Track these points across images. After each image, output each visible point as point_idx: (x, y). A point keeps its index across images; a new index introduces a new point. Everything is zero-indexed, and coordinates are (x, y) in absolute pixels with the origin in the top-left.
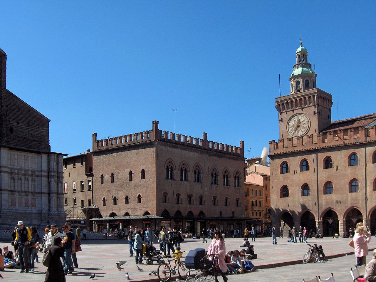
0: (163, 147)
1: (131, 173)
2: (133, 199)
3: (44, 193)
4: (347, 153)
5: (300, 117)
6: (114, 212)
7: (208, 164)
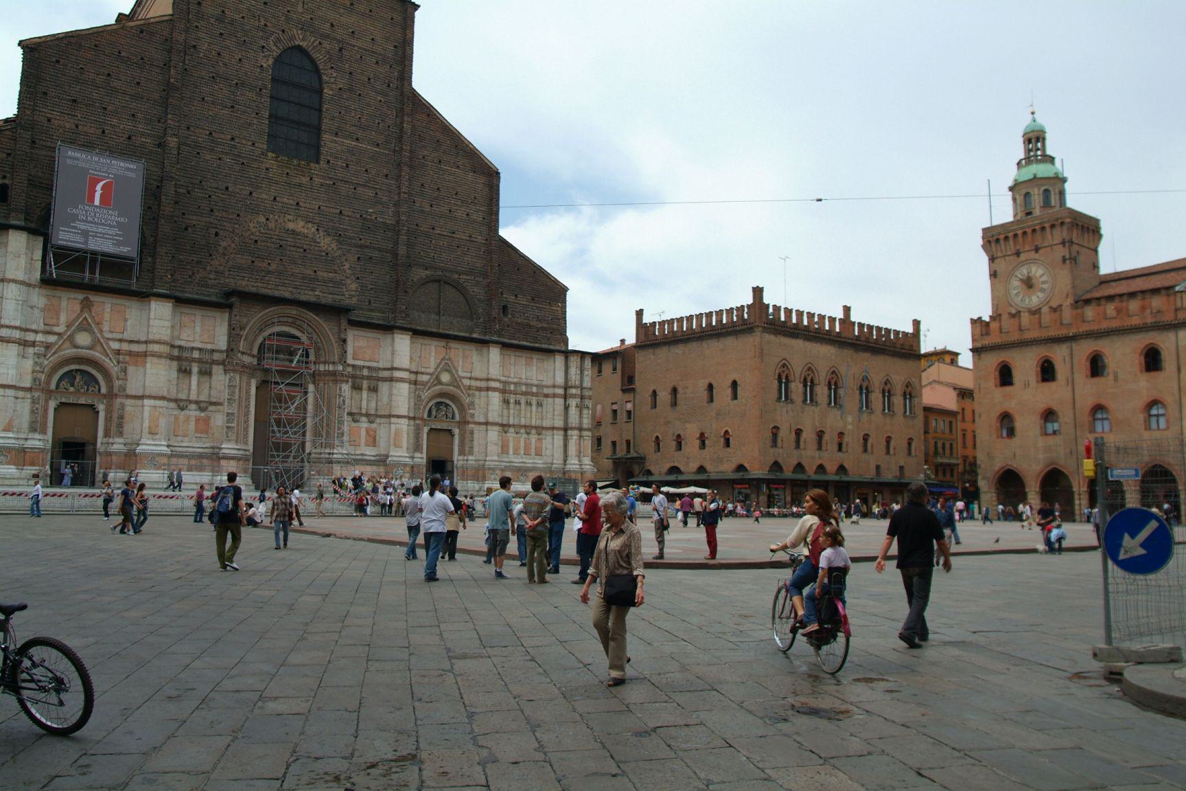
0: (772, 337)
2: (714, 442)
3: (558, 429)
5: (1034, 269)
7: (853, 367)
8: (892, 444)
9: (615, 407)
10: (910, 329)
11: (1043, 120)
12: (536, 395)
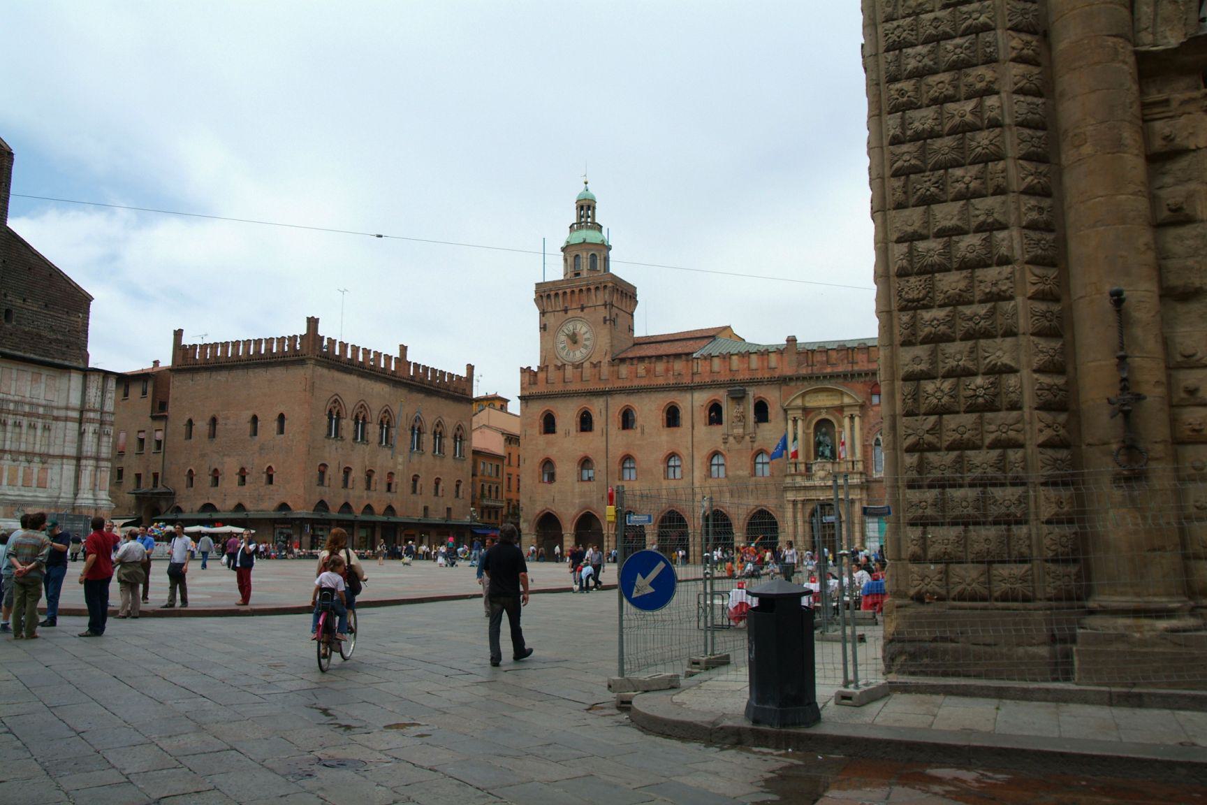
0: (325, 371)
1: (255, 419)
3: (68, 457)
4: (662, 400)
6: (211, 501)
7: (406, 407)
8: (441, 485)
9: (142, 435)
10: (464, 374)
11: (594, 191)
12: (43, 417)
